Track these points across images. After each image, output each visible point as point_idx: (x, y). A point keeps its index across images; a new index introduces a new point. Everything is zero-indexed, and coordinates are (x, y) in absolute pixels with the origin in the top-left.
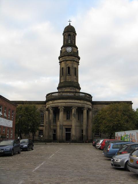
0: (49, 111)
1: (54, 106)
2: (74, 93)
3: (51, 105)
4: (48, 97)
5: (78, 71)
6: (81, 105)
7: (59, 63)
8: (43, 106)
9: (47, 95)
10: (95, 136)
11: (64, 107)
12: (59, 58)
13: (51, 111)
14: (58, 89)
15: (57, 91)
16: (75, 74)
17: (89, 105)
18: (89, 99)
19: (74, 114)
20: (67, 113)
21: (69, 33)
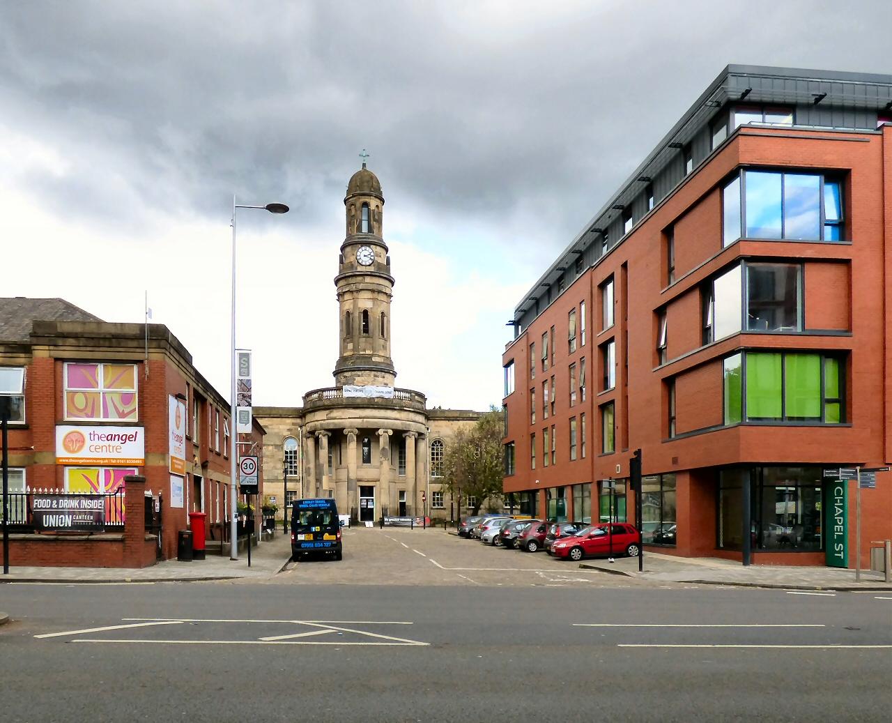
0: (317, 441)
1: (331, 427)
3: (321, 424)
8: (293, 424)
10: (432, 509)
12: (337, 282)
13: (324, 441)
14: (334, 375)
18: (419, 405)
19: (384, 449)
21: (366, 199)
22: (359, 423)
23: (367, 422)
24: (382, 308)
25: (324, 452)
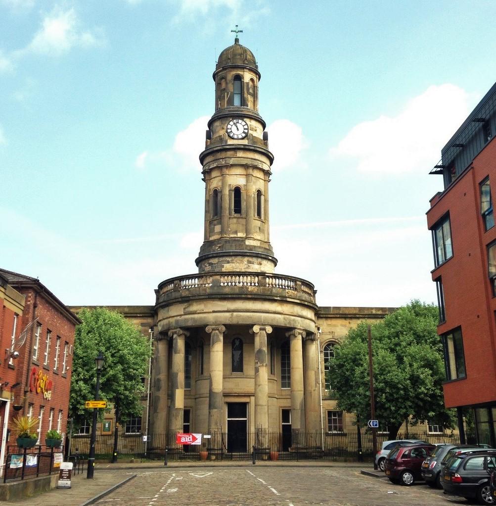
1: (190, 324)
2: (260, 277)
3: (177, 321)
4: (165, 290)
5: (266, 201)
6: (284, 319)
7: (202, 173)
9: (162, 285)
11: (225, 325)
12: (202, 158)
13: (180, 344)
14: (197, 265)
15: (195, 270)
16: (259, 214)
17: (304, 320)
19: (260, 351)
20: (234, 349)
22: (225, 317)
23: (237, 316)
24: (260, 185)
25: (179, 359)
